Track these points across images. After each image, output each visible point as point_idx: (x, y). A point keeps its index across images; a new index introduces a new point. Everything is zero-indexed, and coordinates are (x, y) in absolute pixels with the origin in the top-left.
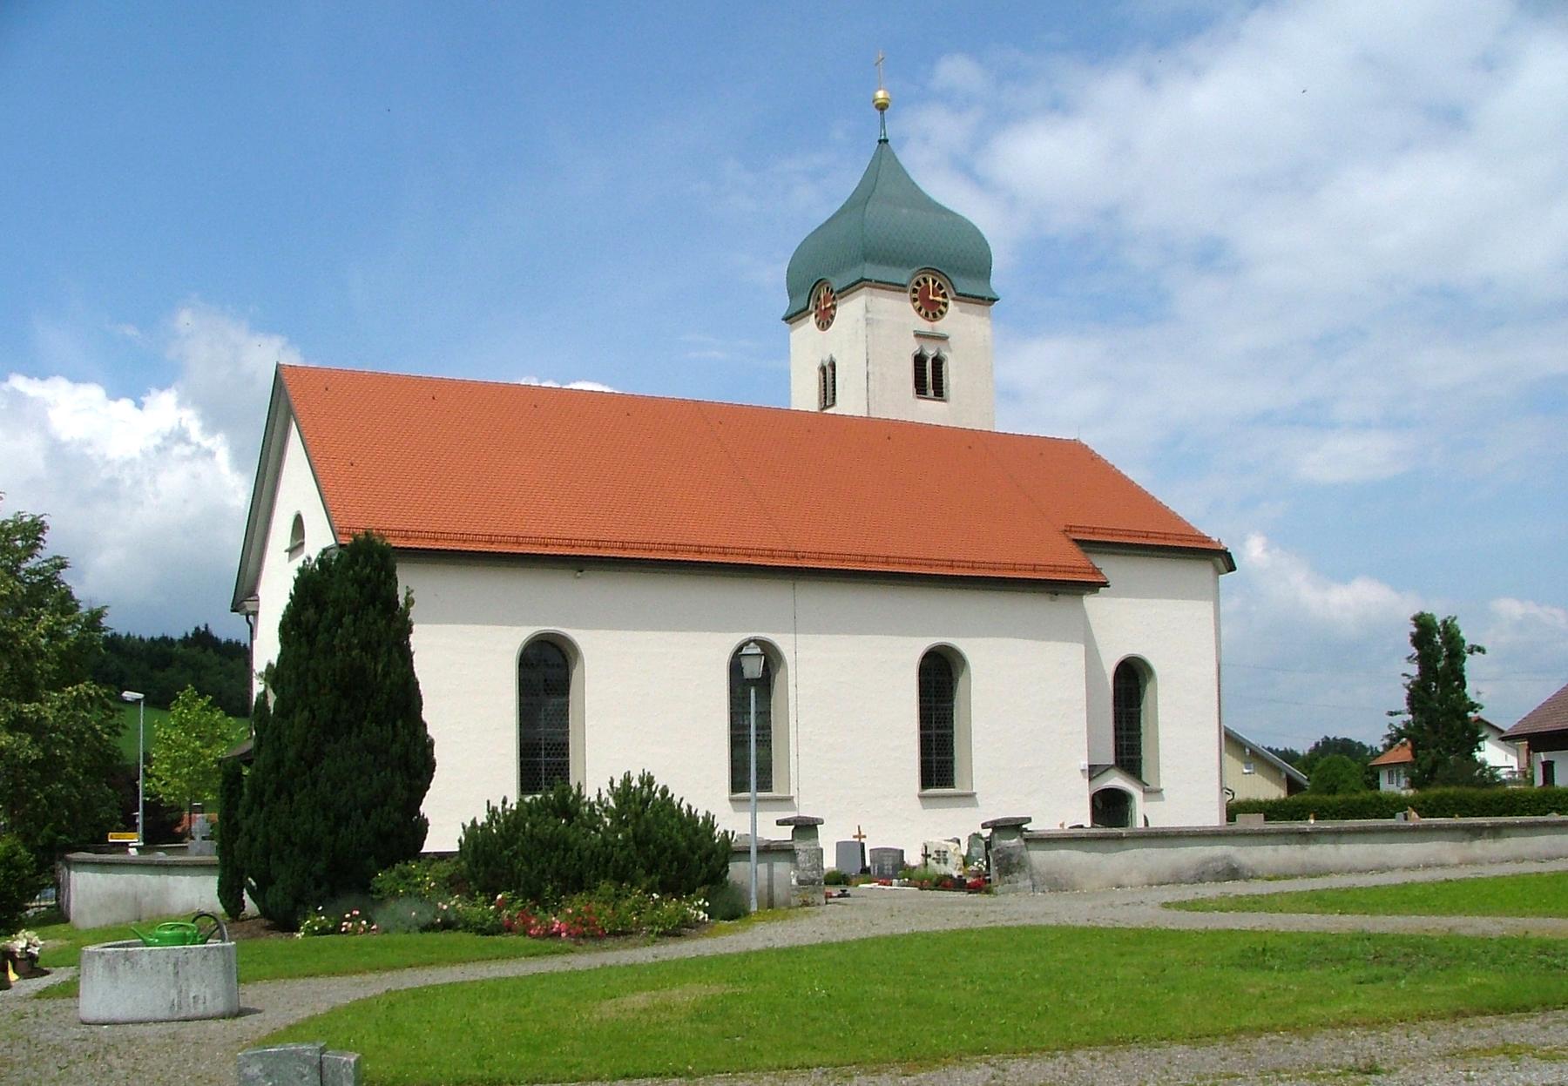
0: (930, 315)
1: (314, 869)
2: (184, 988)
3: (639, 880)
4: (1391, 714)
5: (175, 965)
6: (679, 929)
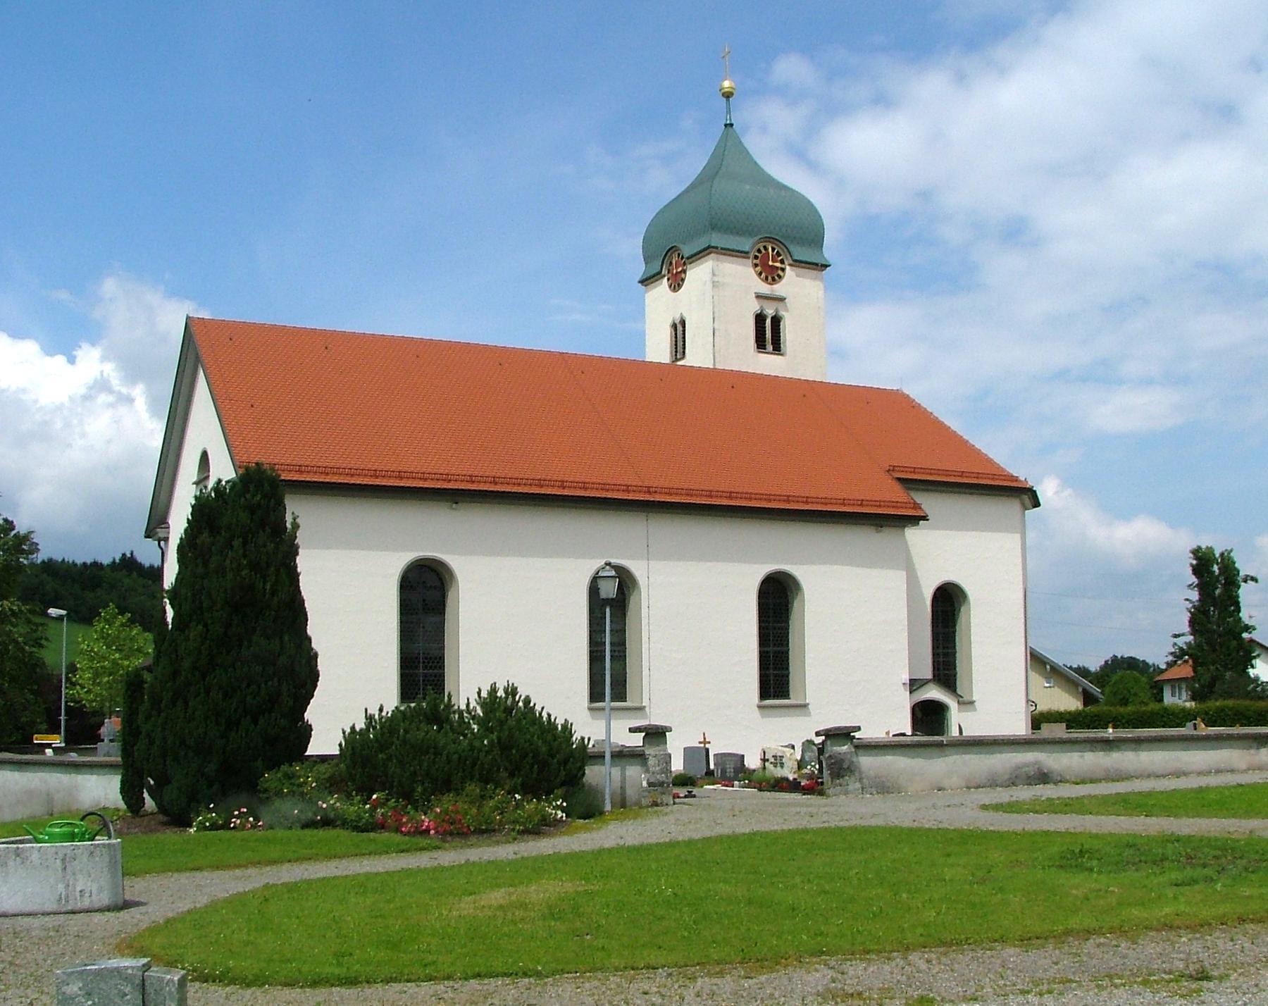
0: (770, 278)
1: (206, 770)
2: (71, 883)
3: (502, 782)
4: (1176, 636)
5: (63, 860)
6: (541, 827)
